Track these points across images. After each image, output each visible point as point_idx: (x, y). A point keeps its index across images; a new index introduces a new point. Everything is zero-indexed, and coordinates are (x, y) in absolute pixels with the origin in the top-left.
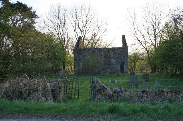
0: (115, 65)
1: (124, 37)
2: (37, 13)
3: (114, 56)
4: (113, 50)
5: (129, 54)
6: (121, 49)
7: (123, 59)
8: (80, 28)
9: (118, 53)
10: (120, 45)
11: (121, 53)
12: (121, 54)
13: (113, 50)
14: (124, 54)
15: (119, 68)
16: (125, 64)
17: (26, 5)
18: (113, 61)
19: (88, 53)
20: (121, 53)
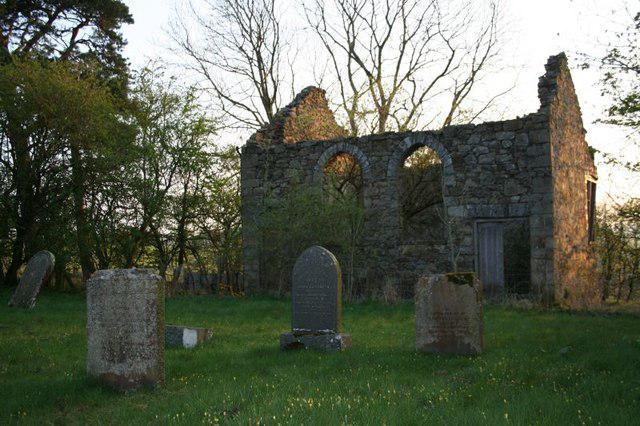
0: (468, 240)
1: (557, 65)
2: (124, 38)
3: (463, 181)
4: (455, 142)
5: (184, 343)
6: (501, 136)
7: (516, 198)
8: (362, 70)
9: (483, 159)
10: (530, 104)
11: (505, 158)
12: (501, 166)
13: (455, 142)
14: (522, 163)
15: (492, 255)
16: (533, 233)
17: (542, 78)
18: (456, 212)
19: (312, 169)
20: (505, 158)
